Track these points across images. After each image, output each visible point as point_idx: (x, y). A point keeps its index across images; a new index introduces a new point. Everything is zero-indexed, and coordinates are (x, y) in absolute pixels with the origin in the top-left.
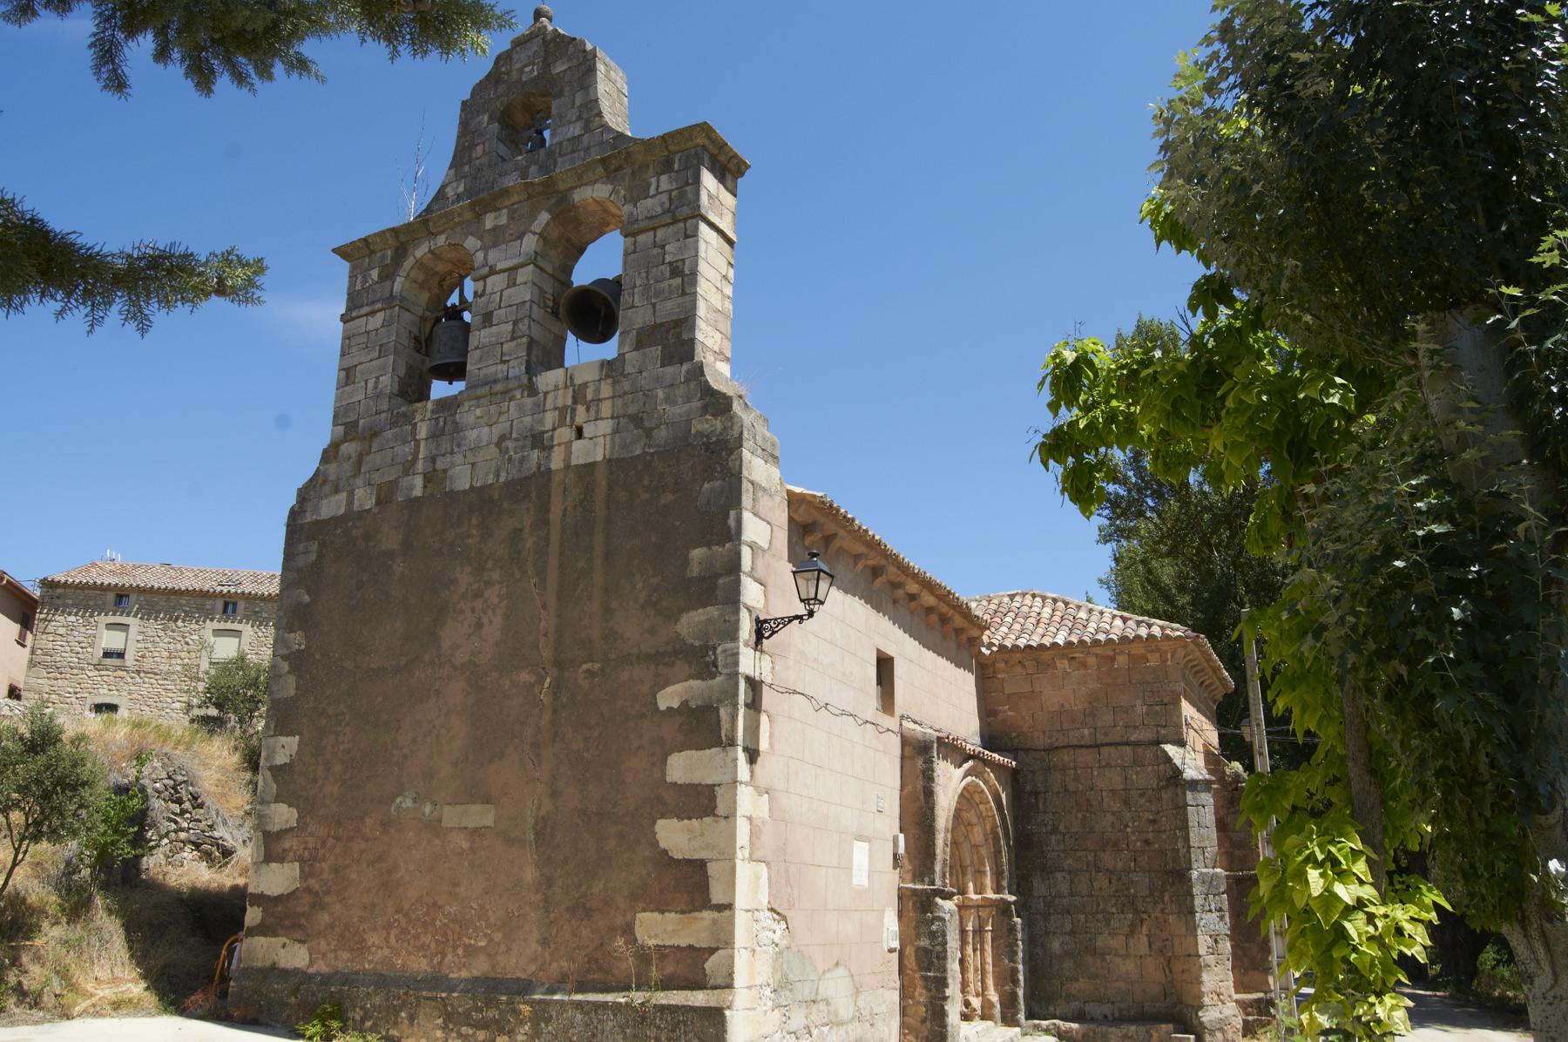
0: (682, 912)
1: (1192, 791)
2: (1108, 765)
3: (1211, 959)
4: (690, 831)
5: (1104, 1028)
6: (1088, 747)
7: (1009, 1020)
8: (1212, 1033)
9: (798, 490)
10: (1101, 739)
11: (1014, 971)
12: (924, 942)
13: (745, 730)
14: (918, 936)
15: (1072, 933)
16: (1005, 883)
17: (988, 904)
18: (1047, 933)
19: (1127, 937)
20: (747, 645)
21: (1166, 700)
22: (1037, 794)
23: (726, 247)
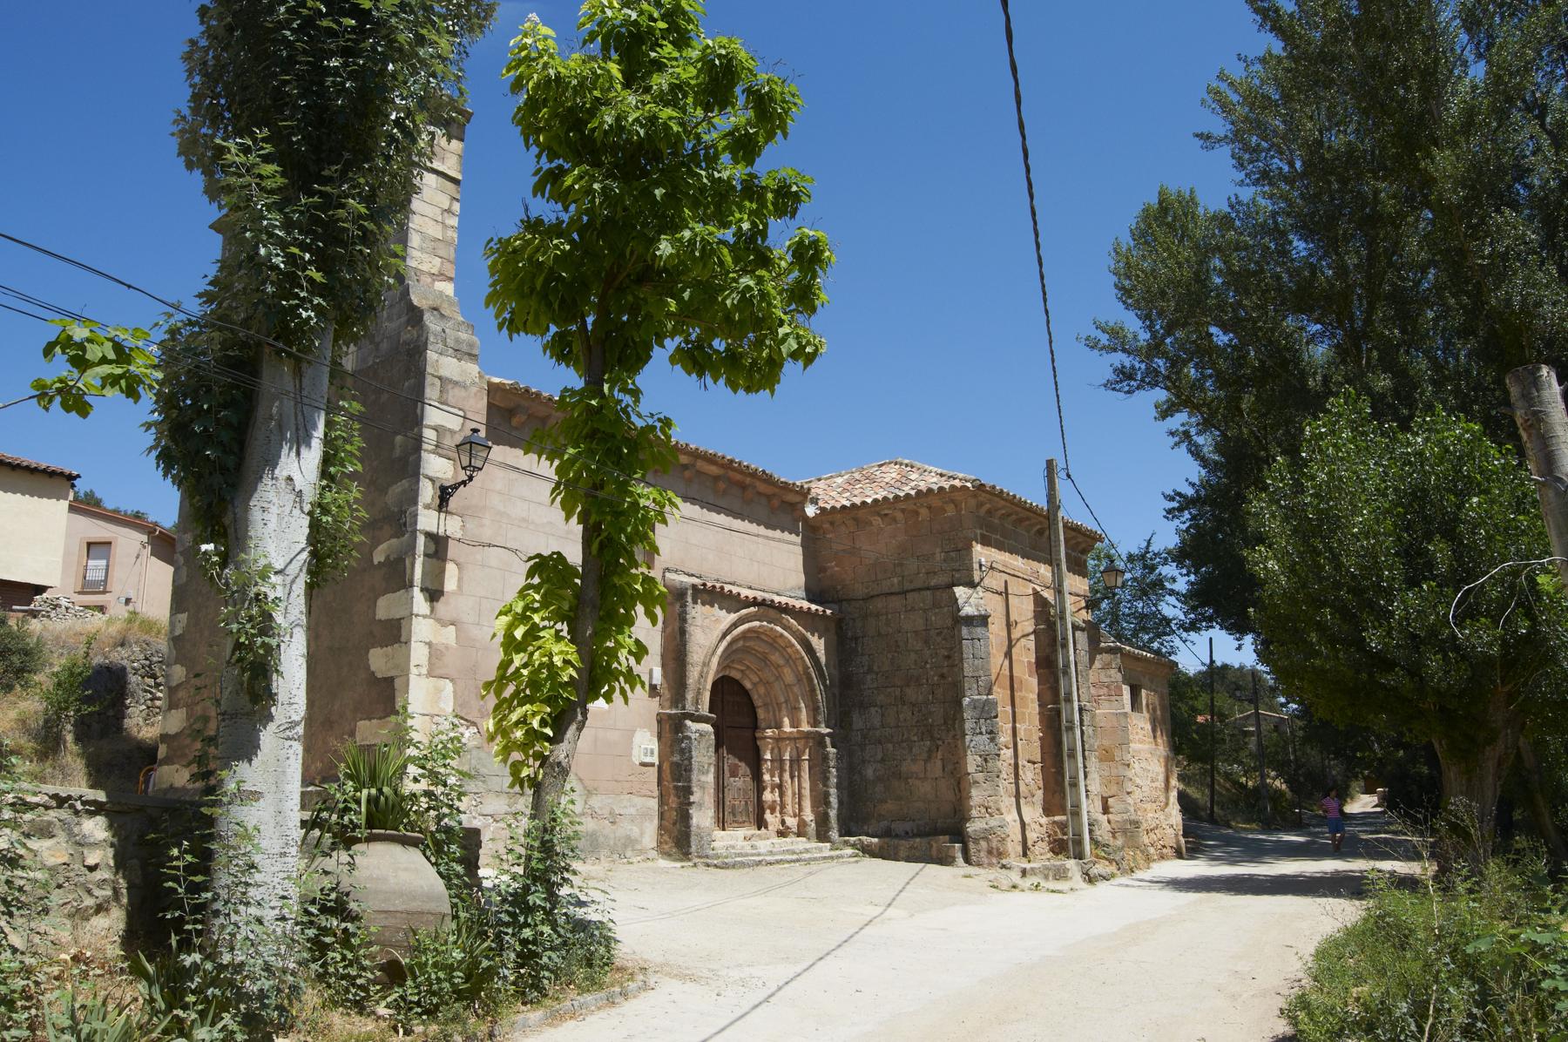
0: (380, 718)
1: (967, 625)
2: (913, 609)
3: (980, 777)
4: (387, 656)
5: (896, 841)
6: (898, 593)
7: (822, 836)
8: (976, 841)
9: (496, 380)
10: (907, 586)
11: (827, 795)
12: (676, 758)
13: (424, 574)
14: (672, 753)
15: (883, 760)
16: (820, 718)
17: (807, 735)
18: (863, 762)
19: (926, 761)
20: (427, 507)
21: (960, 546)
22: (856, 639)
23: (449, 185)
